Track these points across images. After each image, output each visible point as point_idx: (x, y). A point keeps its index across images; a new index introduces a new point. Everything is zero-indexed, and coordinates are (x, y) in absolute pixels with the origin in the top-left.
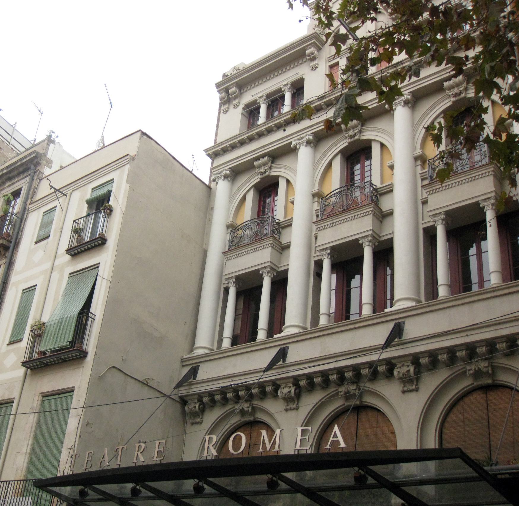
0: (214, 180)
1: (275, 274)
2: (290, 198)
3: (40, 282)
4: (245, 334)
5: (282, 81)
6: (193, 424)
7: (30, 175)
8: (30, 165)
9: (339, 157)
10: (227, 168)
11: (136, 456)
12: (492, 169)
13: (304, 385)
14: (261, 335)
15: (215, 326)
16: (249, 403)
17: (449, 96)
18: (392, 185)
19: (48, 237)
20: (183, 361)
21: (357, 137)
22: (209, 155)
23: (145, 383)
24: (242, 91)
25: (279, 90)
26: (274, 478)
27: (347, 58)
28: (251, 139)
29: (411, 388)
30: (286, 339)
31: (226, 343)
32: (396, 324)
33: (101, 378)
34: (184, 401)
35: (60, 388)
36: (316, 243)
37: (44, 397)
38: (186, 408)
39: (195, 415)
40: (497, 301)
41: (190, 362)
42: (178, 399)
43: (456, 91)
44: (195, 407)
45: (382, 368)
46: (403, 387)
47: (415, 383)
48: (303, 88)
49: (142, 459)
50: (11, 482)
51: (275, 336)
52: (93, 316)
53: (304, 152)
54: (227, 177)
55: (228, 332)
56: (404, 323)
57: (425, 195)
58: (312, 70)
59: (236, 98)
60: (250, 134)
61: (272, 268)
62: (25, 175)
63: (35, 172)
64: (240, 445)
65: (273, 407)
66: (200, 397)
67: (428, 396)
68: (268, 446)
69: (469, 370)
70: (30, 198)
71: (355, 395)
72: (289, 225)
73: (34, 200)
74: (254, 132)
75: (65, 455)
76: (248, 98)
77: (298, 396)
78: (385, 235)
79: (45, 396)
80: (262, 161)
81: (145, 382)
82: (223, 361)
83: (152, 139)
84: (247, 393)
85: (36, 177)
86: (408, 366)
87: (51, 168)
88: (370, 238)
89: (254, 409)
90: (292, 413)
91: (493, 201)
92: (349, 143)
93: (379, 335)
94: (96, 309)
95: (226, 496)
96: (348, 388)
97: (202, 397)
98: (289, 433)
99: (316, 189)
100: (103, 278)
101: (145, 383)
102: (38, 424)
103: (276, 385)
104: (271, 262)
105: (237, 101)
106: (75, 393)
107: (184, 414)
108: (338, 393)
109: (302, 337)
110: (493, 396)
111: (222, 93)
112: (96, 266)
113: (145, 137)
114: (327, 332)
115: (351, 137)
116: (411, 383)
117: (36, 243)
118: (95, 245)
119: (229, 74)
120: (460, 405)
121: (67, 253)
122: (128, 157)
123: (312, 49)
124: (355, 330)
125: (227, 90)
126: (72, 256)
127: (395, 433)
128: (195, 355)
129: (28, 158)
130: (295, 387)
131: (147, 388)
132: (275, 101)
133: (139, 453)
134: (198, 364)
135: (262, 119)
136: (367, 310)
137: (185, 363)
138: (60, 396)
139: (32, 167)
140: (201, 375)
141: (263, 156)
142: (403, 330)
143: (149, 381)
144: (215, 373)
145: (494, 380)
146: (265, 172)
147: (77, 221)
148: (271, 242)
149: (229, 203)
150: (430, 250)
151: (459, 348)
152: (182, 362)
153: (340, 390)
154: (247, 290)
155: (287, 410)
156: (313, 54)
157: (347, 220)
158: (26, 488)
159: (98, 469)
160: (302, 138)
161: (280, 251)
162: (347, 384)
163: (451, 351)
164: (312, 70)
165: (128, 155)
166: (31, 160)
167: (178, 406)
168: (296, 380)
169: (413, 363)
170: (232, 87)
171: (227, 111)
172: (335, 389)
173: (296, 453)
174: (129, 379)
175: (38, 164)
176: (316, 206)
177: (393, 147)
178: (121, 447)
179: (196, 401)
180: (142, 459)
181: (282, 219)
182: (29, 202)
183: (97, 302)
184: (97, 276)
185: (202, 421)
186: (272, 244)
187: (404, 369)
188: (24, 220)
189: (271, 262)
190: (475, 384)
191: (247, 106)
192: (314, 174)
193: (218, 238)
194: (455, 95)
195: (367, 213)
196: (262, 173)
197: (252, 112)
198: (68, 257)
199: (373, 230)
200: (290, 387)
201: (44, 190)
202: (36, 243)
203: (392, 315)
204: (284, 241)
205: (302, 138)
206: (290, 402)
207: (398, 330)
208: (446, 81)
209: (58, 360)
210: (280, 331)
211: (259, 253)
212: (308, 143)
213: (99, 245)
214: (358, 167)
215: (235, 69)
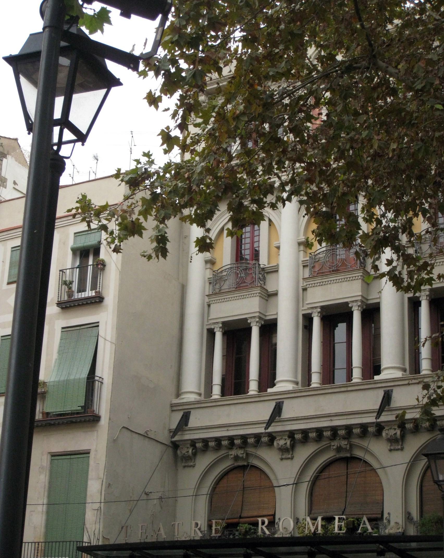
2: (275, 243)
4: (235, 383)
6: (185, 467)
12: (361, 274)
14: (253, 386)
18: (278, 265)
20: (172, 406)
23: (145, 436)
26: (313, 550)
29: (397, 447)
31: (216, 390)
33: (115, 441)
34: (175, 446)
35: (72, 450)
36: (208, 317)
37: (52, 456)
38: (179, 452)
39: (186, 458)
42: (170, 445)
44: (188, 452)
45: (265, 439)
46: (390, 446)
47: (400, 443)
50: (40, 544)
52: (101, 380)
55: (217, 379)
56: (392, 391)
61: (260, 318)
66: (193, 443)
67: (412, 455)
69: (333, 446)
72: (275, 270)
75: (90, 516)
77: (293, 447)
79: (54, 455)
81: (146, 435)
82: (215, 409)
86: (395, 429)
88: (359, 303)
89: (247, 455)
93: (372, 400)
94: (102, 372)
95: (261, 555)
96: (339, 452)
100: (105, 339)
101: (145, 436)
102: (50, 483)
103: (272, 437)
104: (260, 312)
106: (92, 455)
108: (330, 446)
112: (96, 325)
114: (216, 404)
124: (347, 393)
126: (62, 308)
127: (381, 483)
128: (184, 401)
130: (290, 439)
131: (147, 439)
134: (190, 410)
137: (175, 408)
138: (72, 457)
140: (193, 422)
142: (391, 398)
143: (148, 433)
148: (259, 291)
150: (413, 317)
151: (237, 437)
152: (171, 406)
153: (333, 444)
155: (282, 459)
157: (336, 282)
158: (68, 551)
161: (266, 298)
162: (339, 439)
168: (291, 434)
169: (399, 427)
172: (328, 442)
174: (135, 435)
176: (302, 257)
177: (280, 228)
179: (189, 446)
183: (103, 364)
184: (98, 336)
185: (195, 464)
186: (259, 293)
187: (392, 432)
189: (260, 312)
192: (299, 223)
195: (357, 278)
199: (362, 296)
200: (286, 439)
203: (381, 383)
204: (270, 288)
206: (285, 452)
210: (273, 385)
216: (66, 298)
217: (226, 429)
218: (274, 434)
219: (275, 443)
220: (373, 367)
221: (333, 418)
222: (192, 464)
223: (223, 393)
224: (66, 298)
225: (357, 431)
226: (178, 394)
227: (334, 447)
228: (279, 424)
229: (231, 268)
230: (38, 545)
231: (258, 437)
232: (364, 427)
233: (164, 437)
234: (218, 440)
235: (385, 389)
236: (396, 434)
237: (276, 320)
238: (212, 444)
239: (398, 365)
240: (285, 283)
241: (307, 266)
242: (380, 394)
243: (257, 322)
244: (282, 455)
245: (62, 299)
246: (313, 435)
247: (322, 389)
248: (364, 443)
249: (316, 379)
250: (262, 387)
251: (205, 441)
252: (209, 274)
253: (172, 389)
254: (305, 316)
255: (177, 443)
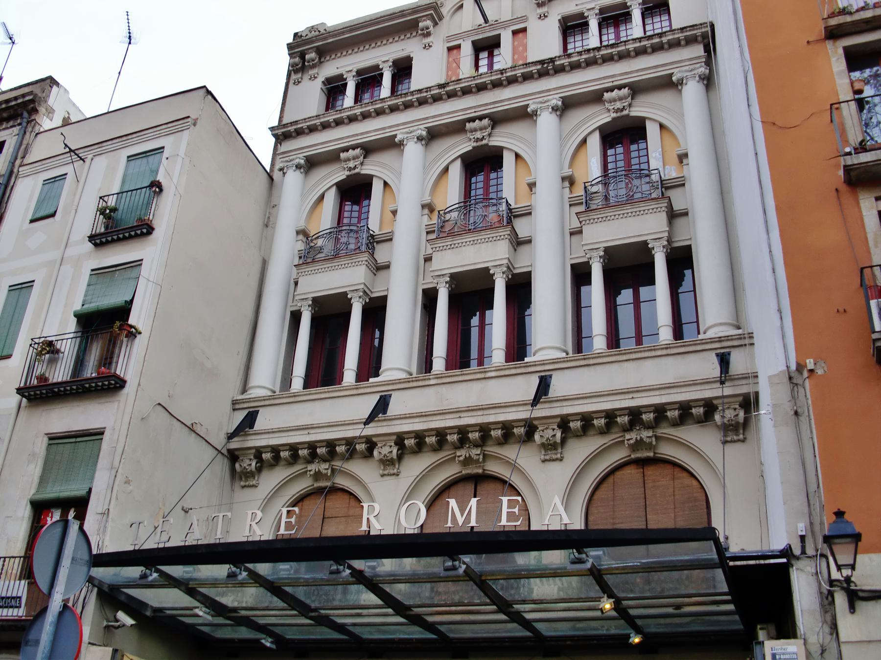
0: (281, 169)
1: (367, 300)
3: (39, 277)
4: (324, 372)
5: (382, 56)
6: (243, 487)
7: (19, 124)
8: (20, 109)
9: (458, 163)
10: (301, 156)
11: (248, 527)
13: (410, 445)
14: (349, 376)
15: (278, 359)
16: (328, 464)
17: (609, 110)
18: (392, 232)
19: (53, 215)
20: (235, 403)
21: (484, 142)
22: (274, 135)
24: (322, 60)
25: (376, 68)
27: (473, 42)
28: (325, 126)
29: (554, 457)
30: (393, 384)
31: (297, 383)
32: (381, 397)
38: (237, 465)
39: (248, 475)
40: (670, 359)
41: (245, 405)
42: (224, 451)
43: (618, 105)
45: (519, 431)
48: (410, 68)
49: (259, 532)
50: (7, 560)
51: (371, 380)
53: (547, 121)
54: (300, 168)
57: (429, 251)
58: (424, 48)
59: (313, 67)
60: (339, 116)
61: (365, 292)
62: (11, 123)
63: (28, 122)
64: (464, 514)
65: (364, 473)
66: (258, 453)
68: (460, 520)
69: (628, 440)
70: (19, 157)
71: (477, 461)
73: (26, 161)
74: (331, 117)
76: (331, 68)
78: (520, 267)
79: (54, 439)
80: (351, 153)
83: (217, 101)
84: (348, 449)
85: (30, 129)
87: (51, 120)
89: (333, 471)
90: (390, 481)
91: (602, 253)
92: (474, 148)
96: (472, 454)
97: (261, 453)
98: (390, 506)
99: (302, 225)
103: (371, 444)
105: (315, 71)
106: (106, 437)
107: (233, 471)
108: (455, 457)
109: (407, 384)
110: (650, 471)
111: (295, 57)
113: (210, 97)
114: (296, 400)
115: (477, 140)
116: (552, 450)
117: (32, 221)
118: (142, 232)
119: (304, 35)
120: (610, 480)
121: (90, 241)
122: (189, 120)
123: (429, 23)
124: (483, 381)
125: (302, 56)
126: (96, 245)
129: (20, 101)
131: (194, 435)
132: (369, 80)
133: (254, 524)
135: (349, 99)
136: (666, 335)
137: (237, 406)
139: (25, 114)
141: (354, 148)
142: (549, 386)
144: (280, 424)
145: (655, 453)
146: (355, 167)
147: (106, 199)
149: (304, 202)
153: (458, 454)
154: (329, 317)
156: (428, 28)
157: (474, 243)
159: (182, 544)
160: (291, 161)
163: (610, 416)
164: (424, 48)
165: (189, 117)
166: (25, 104)
167: (226, 462)
169: (559, 427)
170: (308, 51)
171: (299, 82)
173: (563, 528)
175: (35, 111)
178: (221, 515)
180: (259, 532)
181: (377, 232)
182: (18, 162)
187: (549, 433)
188: (9, 188)
190: (633, 456)
191: (328, 81)
192: (424, 180)
193: (285, 247)
194: (617, 111)
196: (350, 169)
197: (334, 89)
198: (90, 246)
201: (41, 148)
202: (32, 221)
203: (535, 365)
205: (291, 161)
206: (388, 465)
207: (382, 405)
208: (607, 92)
209: (78, 388)
210: (377, 375)
211: (347, 271)
212: (420, 139)
213: (143, 235)
214: (481, 178)
215: (312, 29)
216: (103, 230)
217: (306, 432)
218: (374, 439)
219: (375, 453)
220: (518, 347)
221: (462, 415)
222: (254, 482)
223: (307, 385)
224: (103, 230)
225: (497, 433)
226: (244, 391)
227: (461, 458)
228: (547, 405)
229: (330, 233)
230: (4, 561)
231: (350, 442)
232: (507, 427)
233: (219, 440)
234: (294, 448)
235: (718, 351)
236: (554, 435)
237: (385, 298)
238: (285, 454)
239: (558, 345)
240: (546, 223)
241: (433, 232)
242: (535, 381)
243: (360, 297)
244: (384, 470)
245: (98, 231)
246: (431, 440)
247: (635, 352)
248: (510, 452)
249: (599, 343)
250: (678, 334)
251: (275, 450)
252: (301, 246)
253: (238, 384)
254: (425, 292)
255: (237, 453)
